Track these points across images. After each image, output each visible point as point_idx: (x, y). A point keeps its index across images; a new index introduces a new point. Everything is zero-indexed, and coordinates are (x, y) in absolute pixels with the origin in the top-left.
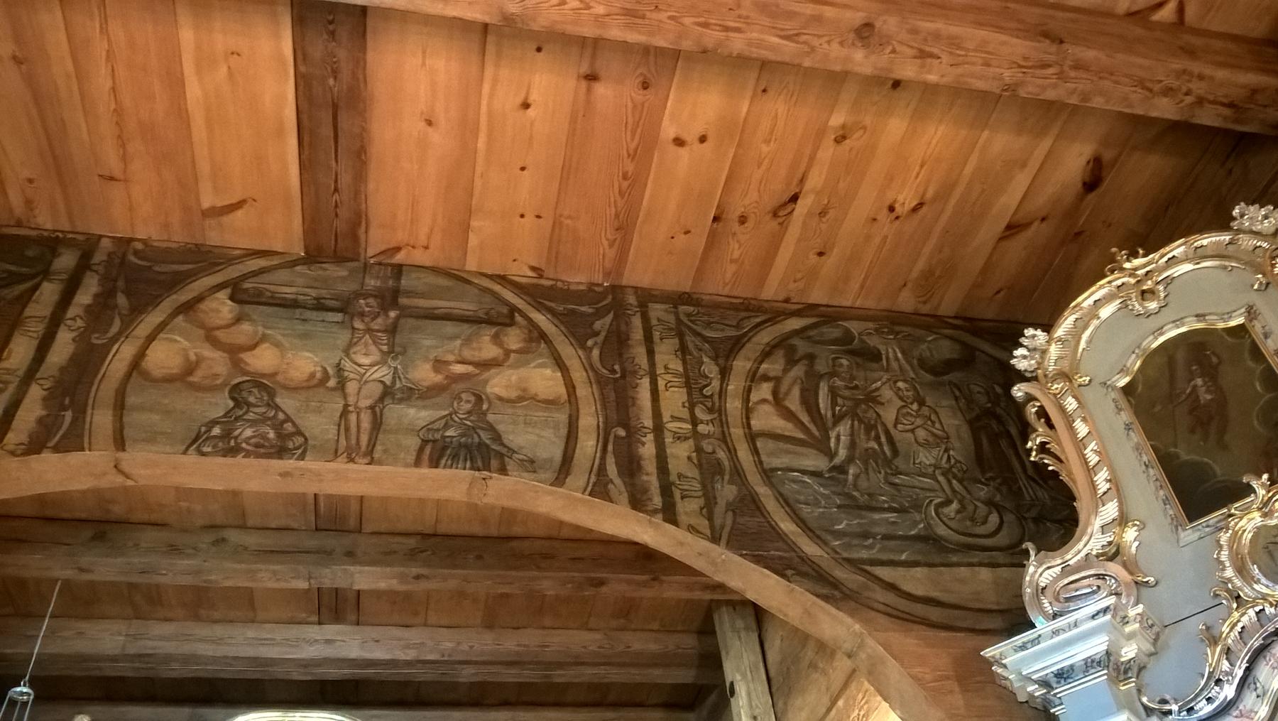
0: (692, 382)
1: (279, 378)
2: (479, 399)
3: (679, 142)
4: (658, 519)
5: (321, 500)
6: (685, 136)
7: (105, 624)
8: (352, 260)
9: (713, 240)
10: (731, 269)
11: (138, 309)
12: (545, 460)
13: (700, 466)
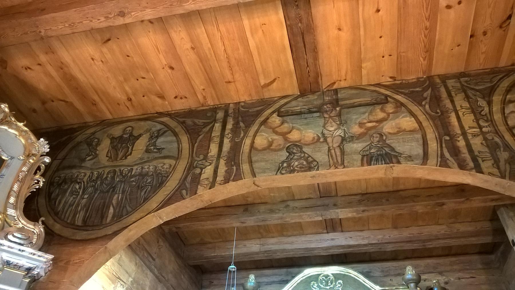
0: (475, 111)
1: (302, 142)
2: (381, 135)
3: (449, 7)
4: (473, 172)
5: (321, 186)
6: (451, 4)
7: (253, 241)
8: (318, 92)
9: (471, 46)
10: (482, 57)
11: (248, 126)
12: (416, 155)
13: (488, 146)
